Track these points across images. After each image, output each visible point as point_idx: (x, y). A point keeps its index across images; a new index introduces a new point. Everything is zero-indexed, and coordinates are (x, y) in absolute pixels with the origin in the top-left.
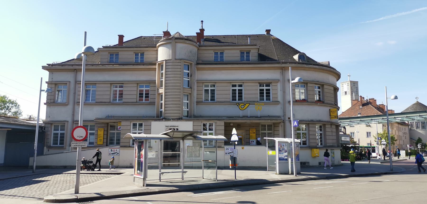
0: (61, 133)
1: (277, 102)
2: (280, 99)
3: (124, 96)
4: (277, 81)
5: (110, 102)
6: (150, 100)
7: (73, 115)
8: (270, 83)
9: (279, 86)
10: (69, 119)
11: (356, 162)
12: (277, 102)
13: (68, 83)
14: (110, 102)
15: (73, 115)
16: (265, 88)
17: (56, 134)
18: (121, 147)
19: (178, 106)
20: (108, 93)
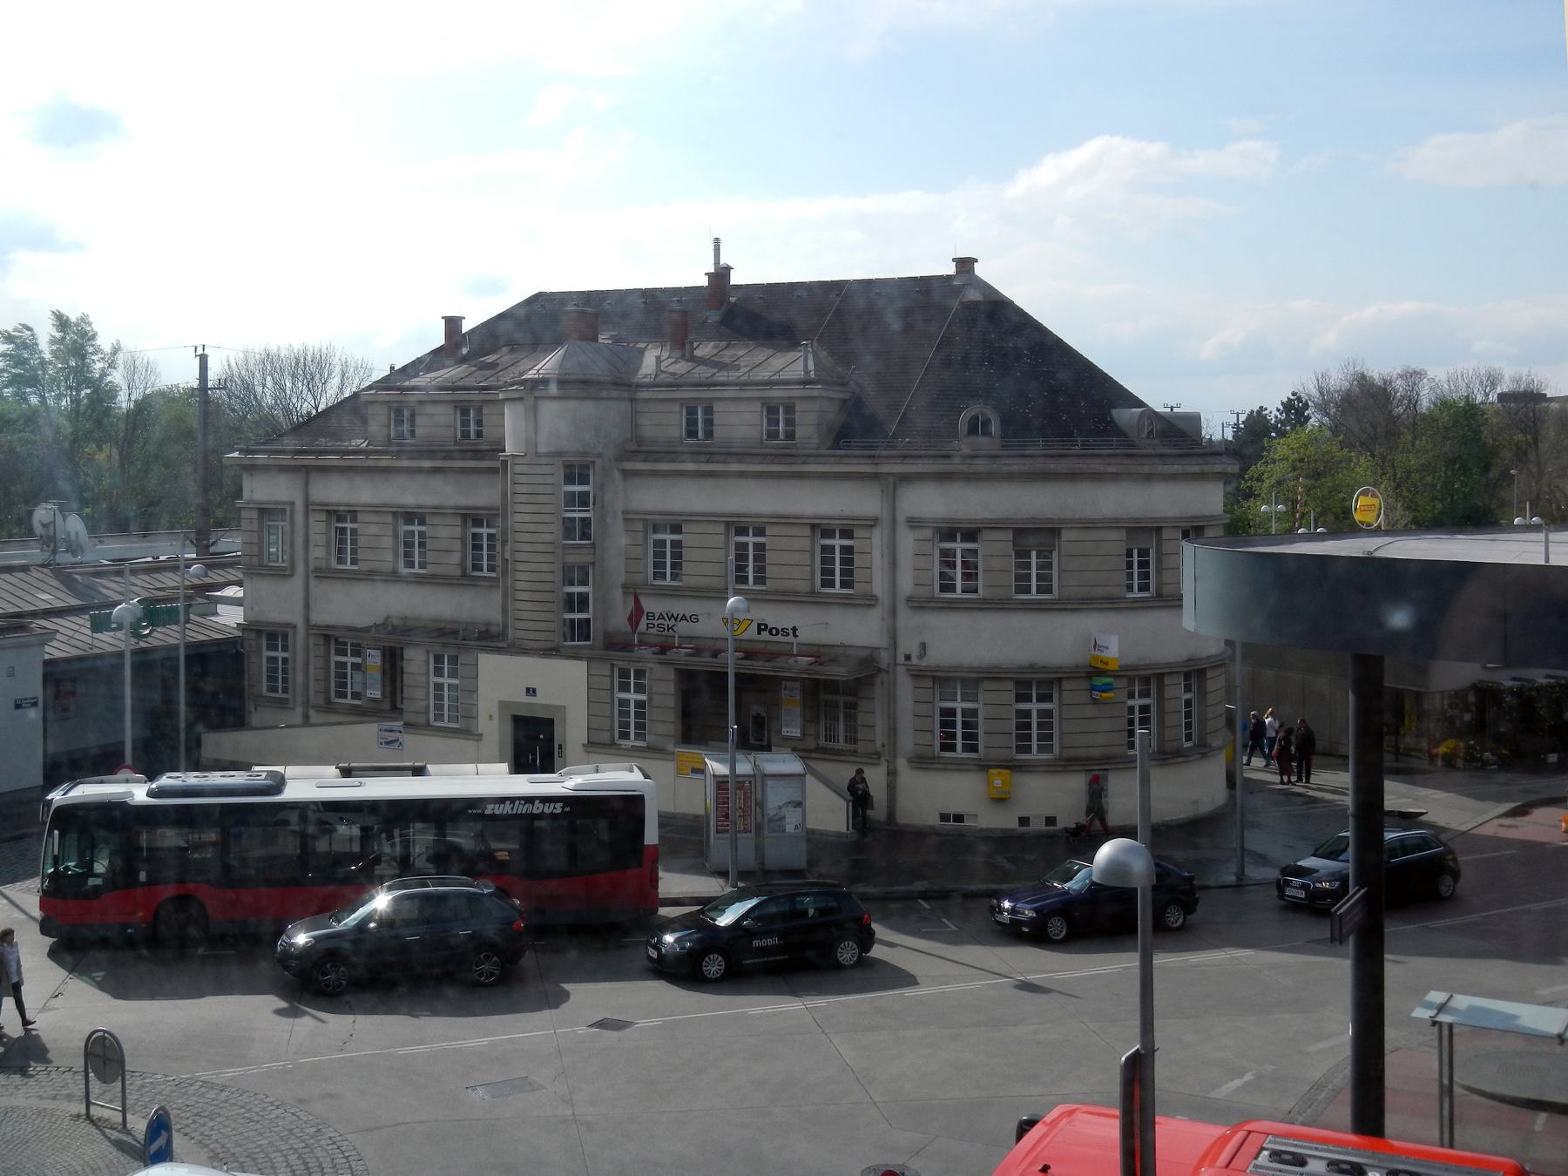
0: (1039, 711)
1: (870, 601)
2: (879, 587)
3: (687, 568)
4: (872, 523)
5: (813, 593)
6: (859, 588)
7: (307, 606)
8: (979, 529)
9: (878, 538)
10: (298, 619)
11: (57, 796)
12: (870, 601)
13: (288, 508)
14: (813, 593)
15: (307, 606)
16: (838, 542)
17: (273, 660)
18: (408, 725)
19: (545, 597)
20: (806, 558)
